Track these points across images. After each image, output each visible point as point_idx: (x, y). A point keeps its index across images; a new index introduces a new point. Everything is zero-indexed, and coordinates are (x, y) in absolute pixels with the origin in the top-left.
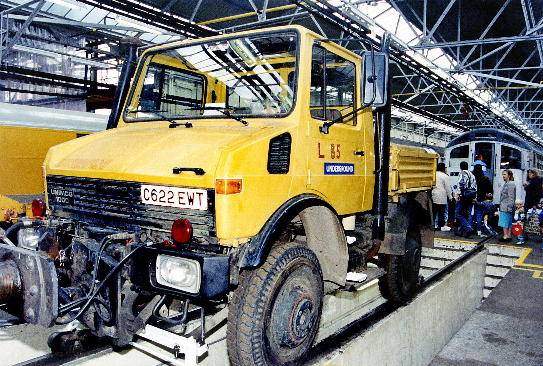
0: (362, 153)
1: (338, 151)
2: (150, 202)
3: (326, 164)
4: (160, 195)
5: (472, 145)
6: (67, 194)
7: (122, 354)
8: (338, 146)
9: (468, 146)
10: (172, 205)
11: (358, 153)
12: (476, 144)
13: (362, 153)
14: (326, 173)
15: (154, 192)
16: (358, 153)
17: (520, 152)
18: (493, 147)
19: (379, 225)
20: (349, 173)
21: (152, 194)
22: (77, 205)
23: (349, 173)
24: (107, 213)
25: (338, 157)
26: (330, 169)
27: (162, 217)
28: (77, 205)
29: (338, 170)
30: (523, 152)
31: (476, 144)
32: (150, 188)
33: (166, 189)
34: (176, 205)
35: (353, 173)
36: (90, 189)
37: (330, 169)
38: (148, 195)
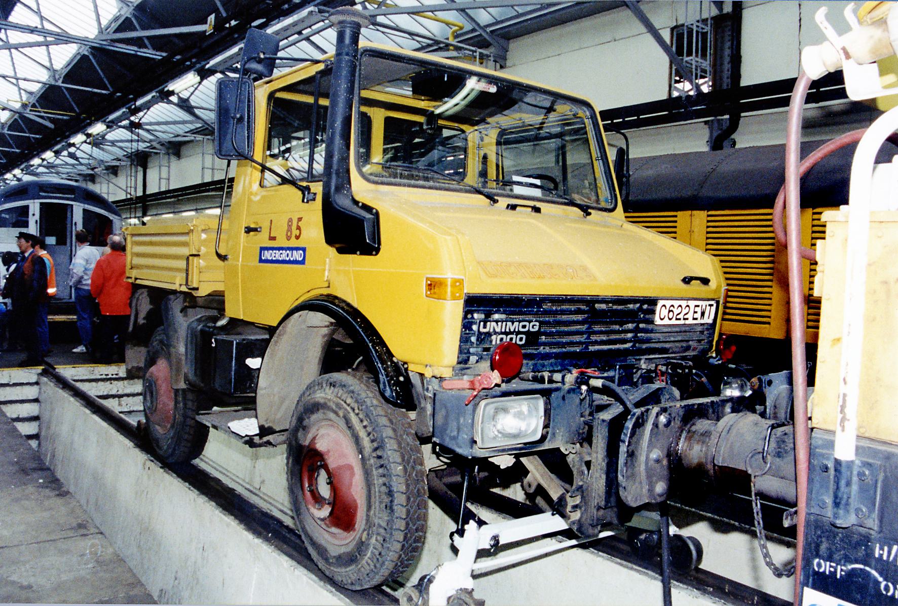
0: (249, 230)
1: (299, 228)
2: (666, 322)
3: (263, 249)
4: (676, 311)
5: (34, 207)
6: (524, 327)
7: (355, 501)
8: (300, 219)
9: (27, 207)
10: (687, 322)
11: (255, 230)
12: (41, 204)
13: (249, 230)
14: (261, 261)
15: (672, 308)
16: (255, 230)
17: (111, 221)
18: (69, 210)
19: (131, 329)
20: (296, 262)
21: (670, 311)
22: (544, 344)
23: (296, 262)
24: (597, 347)
25: (297, 237)
26: (267, 255)
27: (672, 339)
28: (544, 344)
29: (278, 257)
30: (115, 220)
31: (41, 204)
32: (668, 303)
33: (683, 303)
34: (690, 321)
35: (302, 262)
36: (578, 312)
37: (267, 255)
38: (665, 312)
